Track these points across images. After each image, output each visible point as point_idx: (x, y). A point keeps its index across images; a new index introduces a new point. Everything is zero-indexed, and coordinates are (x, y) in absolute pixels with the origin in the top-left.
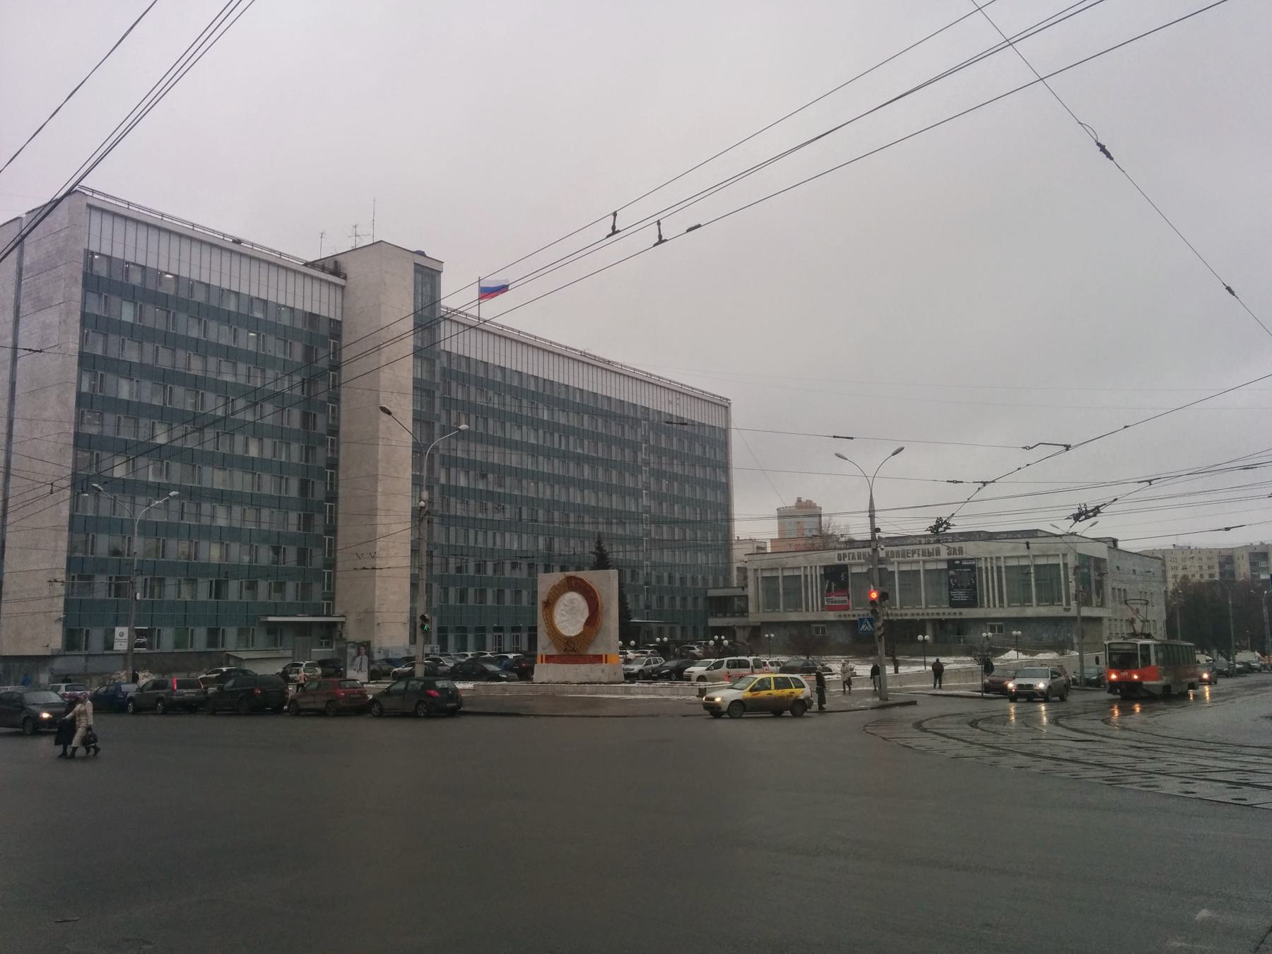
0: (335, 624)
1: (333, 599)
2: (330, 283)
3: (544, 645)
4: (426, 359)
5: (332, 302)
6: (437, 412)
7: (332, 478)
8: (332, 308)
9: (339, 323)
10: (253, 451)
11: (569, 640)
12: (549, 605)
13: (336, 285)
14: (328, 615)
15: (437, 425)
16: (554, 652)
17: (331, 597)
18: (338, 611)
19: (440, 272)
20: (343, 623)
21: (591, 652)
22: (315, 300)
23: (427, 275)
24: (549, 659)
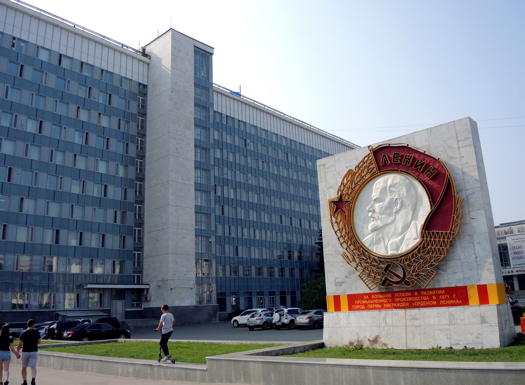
0: (142, 290)
1: (141, 272)
2: (140, 60)
3: (340, 275)
4: (203, 191)
5: (141, 72)
6: (213, 206)
7: (141, 166)
8: (141, 77)
9: (145, 86)
10: (98, 270)
11: (389, 264)
12: (342, 206)
13: (144, 62)
14: (138, 283)
15: (213, 216)
16: (361, 288)
17: (140, 271)
18: (145, 280)
19: (212, 54)
20: (148, 289)
21: (450, 279)
22: (135, 73)
23: (203, 56)
24: (355, 301)
